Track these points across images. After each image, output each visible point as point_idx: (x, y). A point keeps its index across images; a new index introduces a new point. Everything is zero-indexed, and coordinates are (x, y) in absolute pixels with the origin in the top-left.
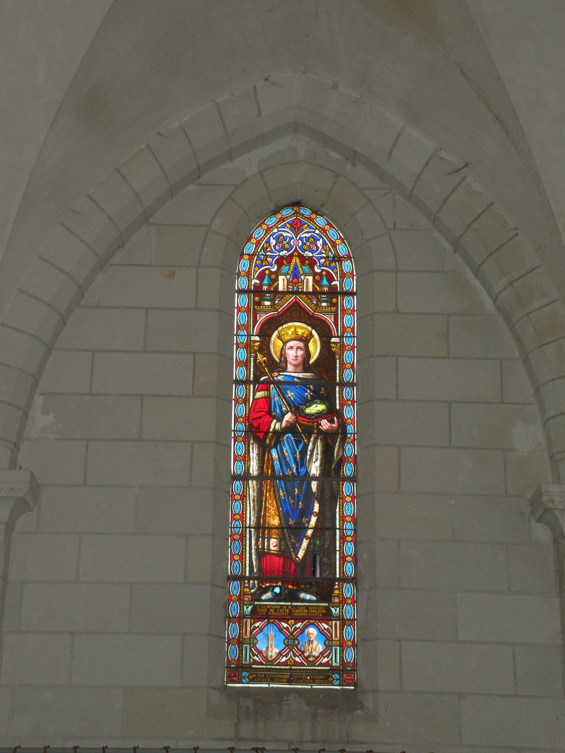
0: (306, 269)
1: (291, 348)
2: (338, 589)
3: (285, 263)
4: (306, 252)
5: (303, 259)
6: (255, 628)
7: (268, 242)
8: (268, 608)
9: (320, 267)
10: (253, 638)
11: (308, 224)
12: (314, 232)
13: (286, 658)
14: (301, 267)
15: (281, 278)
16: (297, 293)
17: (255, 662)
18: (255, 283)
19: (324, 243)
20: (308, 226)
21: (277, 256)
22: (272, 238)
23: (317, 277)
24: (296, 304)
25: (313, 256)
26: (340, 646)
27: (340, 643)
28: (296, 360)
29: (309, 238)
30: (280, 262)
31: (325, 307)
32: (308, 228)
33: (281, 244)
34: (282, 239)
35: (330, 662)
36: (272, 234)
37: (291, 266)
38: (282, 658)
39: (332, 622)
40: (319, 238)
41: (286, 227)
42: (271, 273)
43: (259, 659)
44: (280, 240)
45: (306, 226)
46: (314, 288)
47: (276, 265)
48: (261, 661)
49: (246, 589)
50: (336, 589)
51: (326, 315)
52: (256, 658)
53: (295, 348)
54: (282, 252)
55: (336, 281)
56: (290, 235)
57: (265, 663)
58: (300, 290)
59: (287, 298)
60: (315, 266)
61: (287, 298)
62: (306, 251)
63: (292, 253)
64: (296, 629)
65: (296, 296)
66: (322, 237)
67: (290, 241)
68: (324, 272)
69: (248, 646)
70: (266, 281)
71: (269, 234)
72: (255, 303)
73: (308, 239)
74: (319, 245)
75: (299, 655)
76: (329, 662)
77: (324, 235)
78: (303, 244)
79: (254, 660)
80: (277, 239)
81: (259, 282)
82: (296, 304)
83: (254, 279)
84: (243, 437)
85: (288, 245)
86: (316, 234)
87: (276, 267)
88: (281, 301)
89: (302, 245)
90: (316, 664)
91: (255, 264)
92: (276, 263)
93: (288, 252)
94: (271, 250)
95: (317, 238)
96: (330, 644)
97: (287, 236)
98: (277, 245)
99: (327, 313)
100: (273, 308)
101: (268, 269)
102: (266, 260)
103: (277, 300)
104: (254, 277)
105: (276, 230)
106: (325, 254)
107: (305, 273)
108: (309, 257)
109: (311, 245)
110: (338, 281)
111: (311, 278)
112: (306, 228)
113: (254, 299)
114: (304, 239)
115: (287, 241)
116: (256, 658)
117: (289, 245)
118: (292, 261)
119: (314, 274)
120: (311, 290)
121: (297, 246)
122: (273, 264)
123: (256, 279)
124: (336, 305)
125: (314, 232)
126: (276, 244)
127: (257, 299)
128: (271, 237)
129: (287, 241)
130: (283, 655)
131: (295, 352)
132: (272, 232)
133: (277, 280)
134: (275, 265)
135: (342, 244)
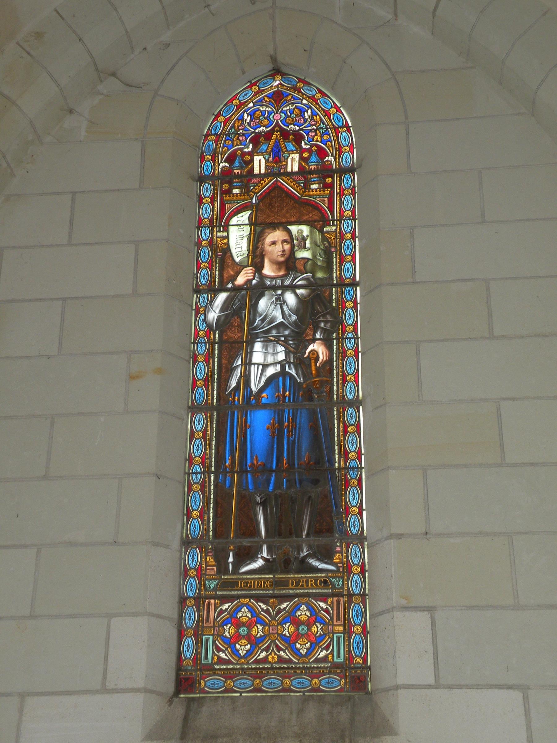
0: (290, 146)
1: (274, 243)
2: (341, 552)
3: (262, 141)
4: (290, 126)
5: (285, 135)
6: (222, 612)
7: (241, 119)
8: (246, 581)
9: (309, 142)
10: (219, 627)
11: (292, 95)
12: (301, 103)
13: (327, 651)
14: (284, 143)
15: (257, 159)
16: (280, 175)
17: (221, 661)
18: (223, 167)
19: (314, 114)
20: (292, 97)
21: (251, 134)
22: (246, 115)
23: (306, 155)
24: (276, 187)
25: (300, 129)
26: (344, 633)
27: (344, 629)
28: (283, 255)
29: (294, 109)
30: (256, 140)
31: (316, 189)
32: (293, 99)
33: (257, 120)
34: (259, 114)
35: (330, 657)
36: (246, 109)
37: (271, 143)
38: (321, 651)
39: (333, 599)
40: (307, 109)
41: (264, 100)
42: (244, 154)
43: (287, 655)
44: (256, 116)
45: (290, 97)
46: (300, 166)
47: (251, 144)
48: (229, 658)
49: (209, 558)
50: (338, 552)
51: (317, 199)
52: (282, 653)
53: (280, 243)
54: (258, 129)
55: (330, 157)
56: (270, 109)
57: (297, 661)
58: (282, 171)
59: (265, 182)
60: (303, 141)
61: (265, 182)
62: (291, 124)
63: (273, 130)
64: (280, 611)
65: (277, 178)
66: (310, 107)
67: (270, 116)
68: (315, 147)
69: (341, 636)
70: (237, 163)
71: (243, 109)
72: (223, 192)
73: (292, 111)
74: (307, 117)
75: (260, 649)
76: (269, 657)
77: (313, 105)
78: (286, 117)
79: (219, 658)
80: (252, 114)
81: (228, 165)
82: (276, 187)
83: (221, 162)
84: (205, 356)
85: (267, 120)
86: (304, 104)
87: (251, 146)
88: (258, 186)
89: (285, 119)
90: (250, 662)
91: (223, 144)
92: (251, 141)
93: (266, 128)
94: (245, 128)
95: (305, 109)
96: (216, 629)
97: (265, 111)
98: (253, 121)
99: (318, 197)
100: (246, 197)
101: (241, 149)
102: (238, 139)
103: (252, 186)
104: (222, 160)
105: (251, 105)
106: (315, 127)
107: (290, 151)
108: (293, 131)
109: (297, 118)
110: (332, 156)
111: (296, 156)
112: (290, 99)
113: (221, 187)
114: (288, 111)
115: (266, 116)
116: (222, 655)
117: (268, 120)
118: (272, 138)
119: (301, 151)
120: (296, 169)
121: (279, 121)
122: (247, 143)
123: (225, 162)
124: (331, 186)
125: (301, 103)
126: (251, 120)
127: (226, 186)
128: (245, 113)
129: (266, 116)
130: (262, 648)
131: (281, 246)
132: (246, 108)
133: (252, 161)
134: (250, 145)
135: (328, 109)
